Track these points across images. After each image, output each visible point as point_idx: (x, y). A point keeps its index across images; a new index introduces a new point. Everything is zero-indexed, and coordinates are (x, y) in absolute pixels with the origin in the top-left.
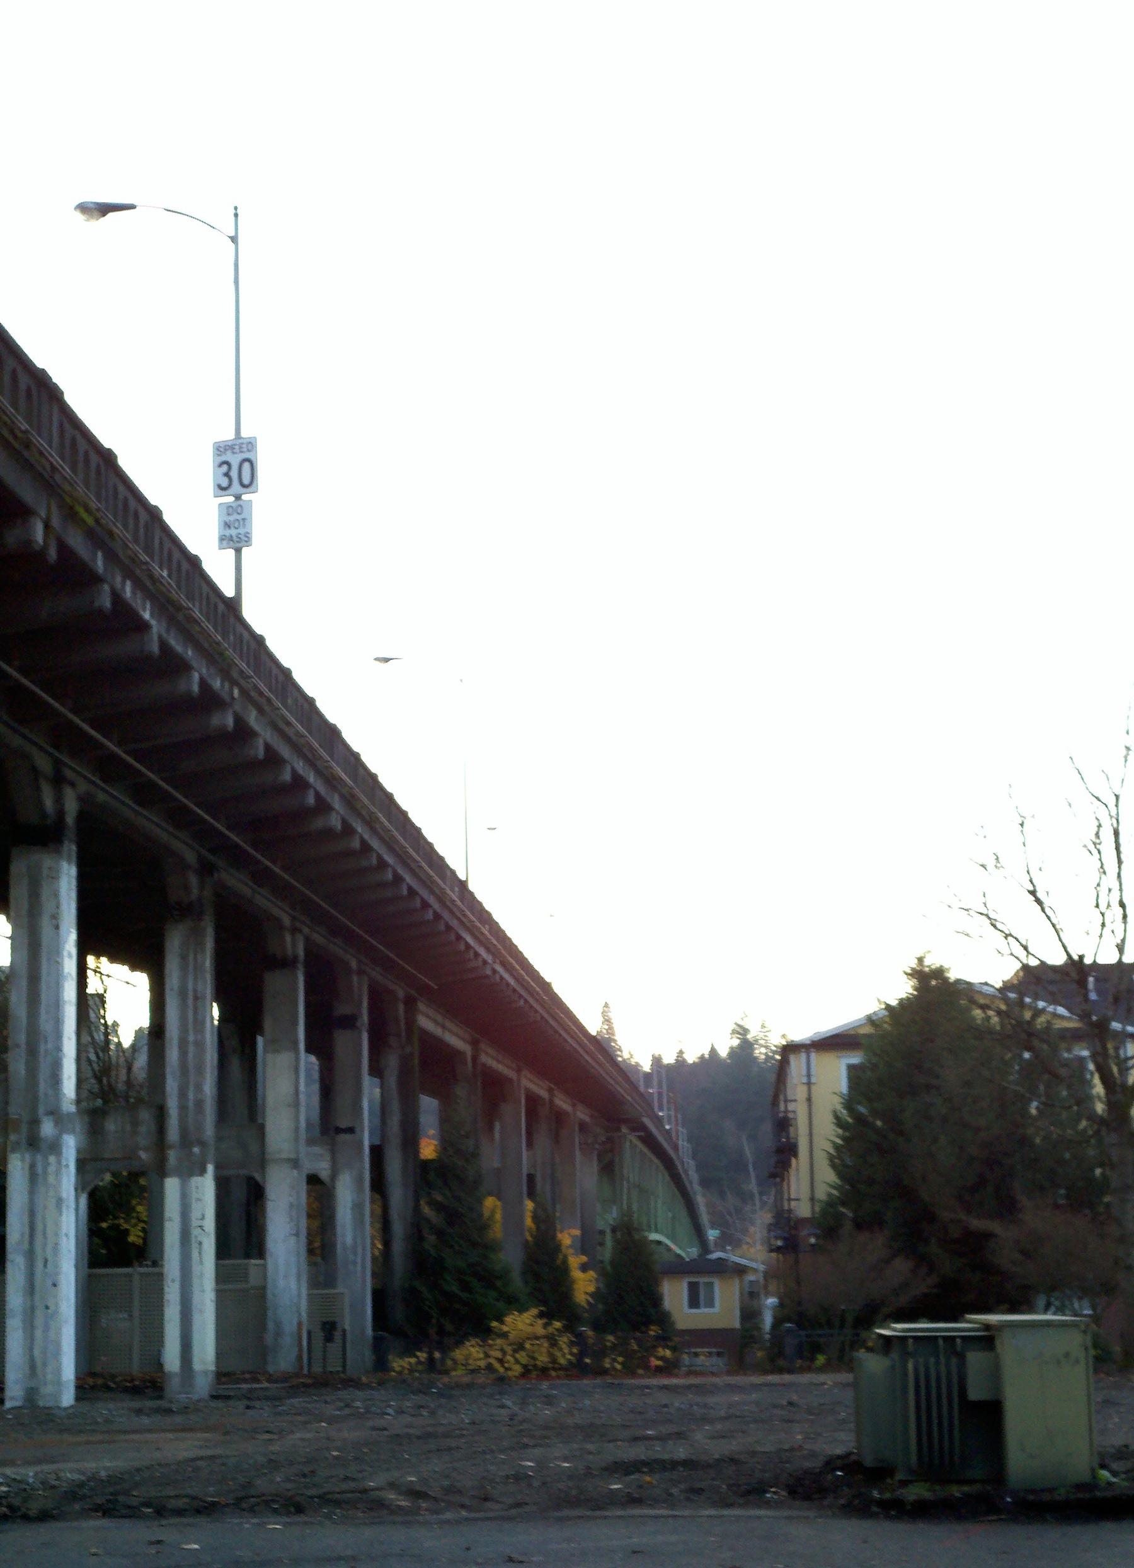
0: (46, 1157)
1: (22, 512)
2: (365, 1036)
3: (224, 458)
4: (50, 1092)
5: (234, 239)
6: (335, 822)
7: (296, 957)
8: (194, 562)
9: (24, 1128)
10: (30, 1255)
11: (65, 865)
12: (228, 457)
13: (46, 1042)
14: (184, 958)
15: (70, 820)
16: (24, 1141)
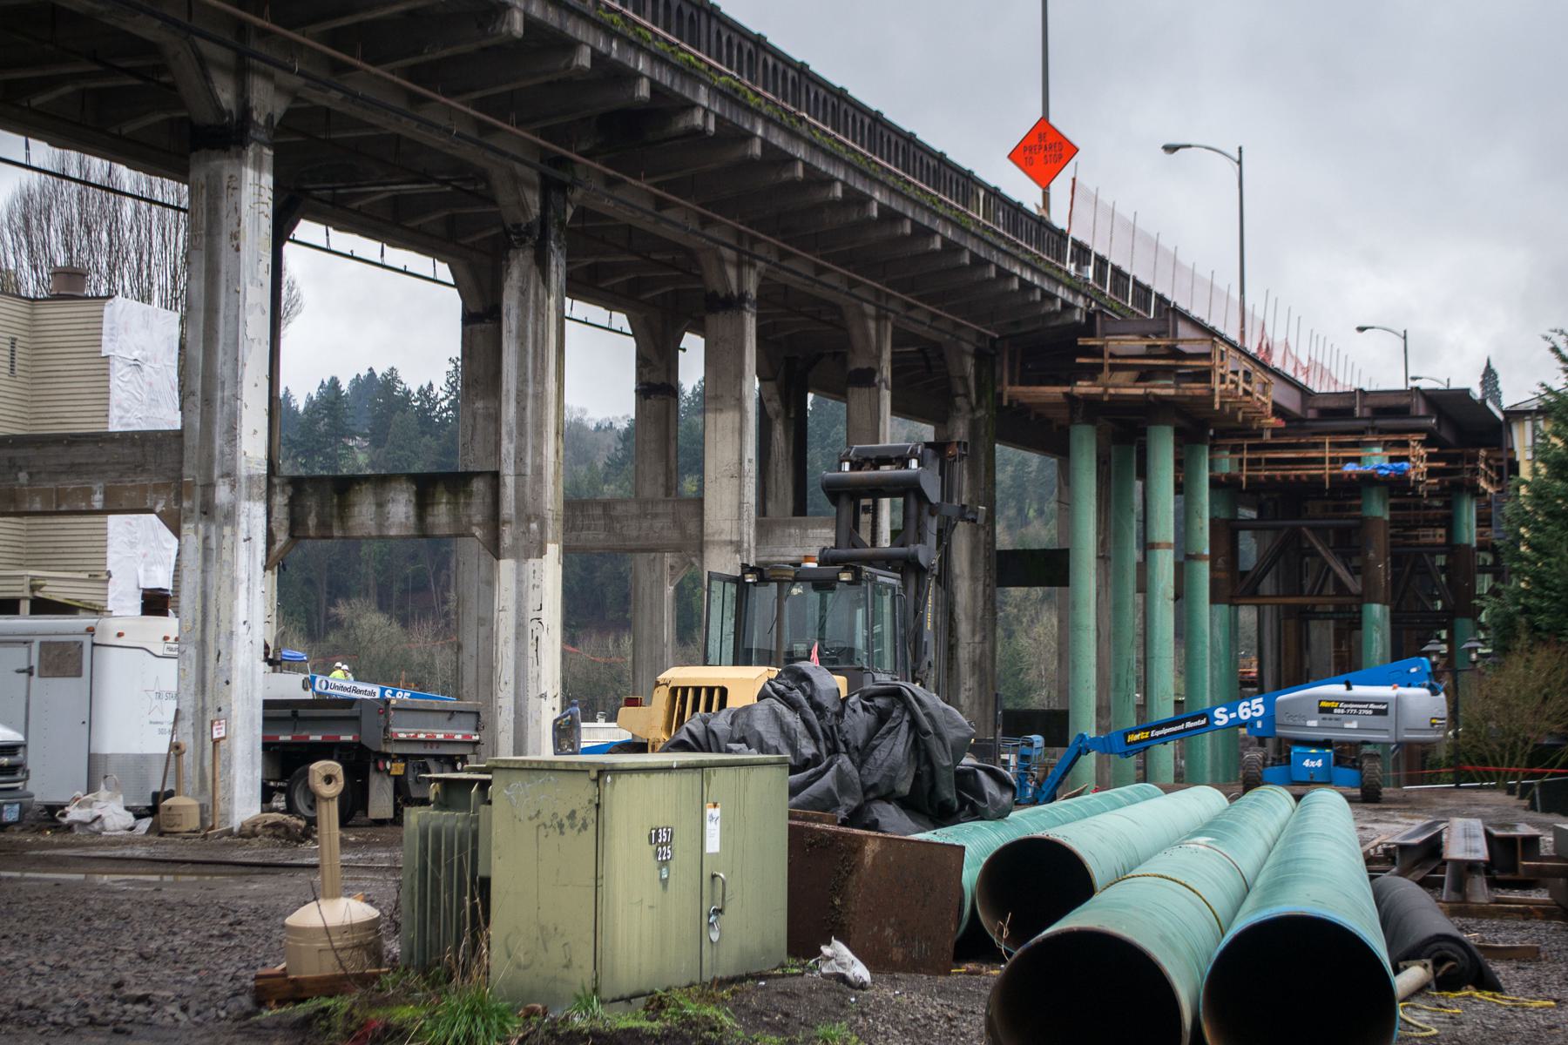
0: (220, 527)
4: (227, 450)
5: (1240, 163)
7: (742, 297)
9: (198, 491)
11: (249, 174)
13: (223, 390)
14: (523, 292)
16: (197, 510)
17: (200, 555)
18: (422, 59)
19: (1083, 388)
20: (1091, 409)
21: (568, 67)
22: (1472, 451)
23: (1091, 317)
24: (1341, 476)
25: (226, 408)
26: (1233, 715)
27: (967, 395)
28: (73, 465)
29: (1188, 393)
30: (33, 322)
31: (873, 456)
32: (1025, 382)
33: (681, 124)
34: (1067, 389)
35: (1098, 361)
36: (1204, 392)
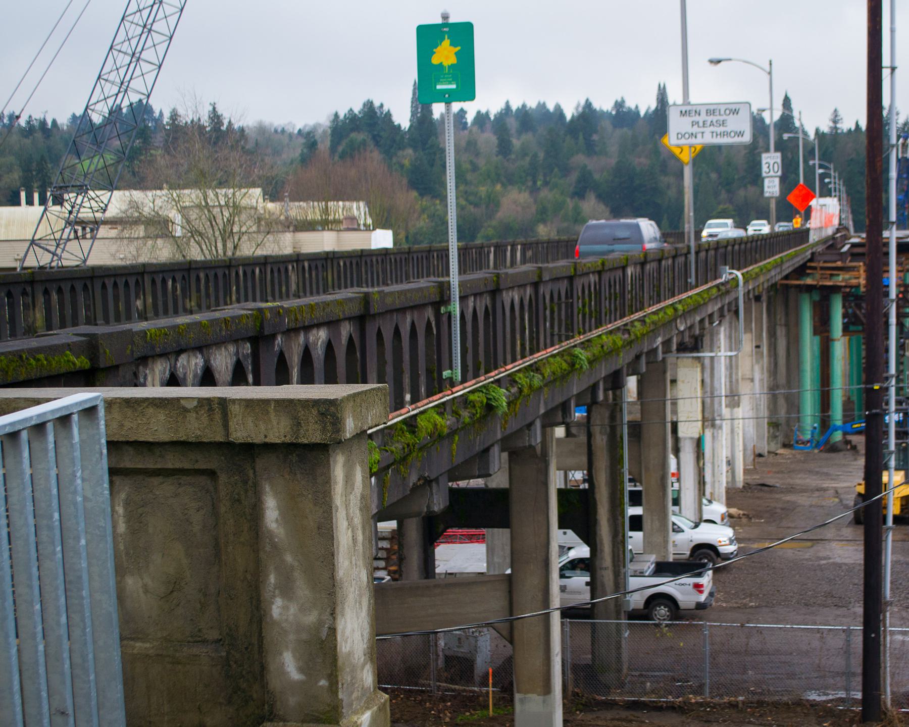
5: (770, 73)
10: (713, 463)
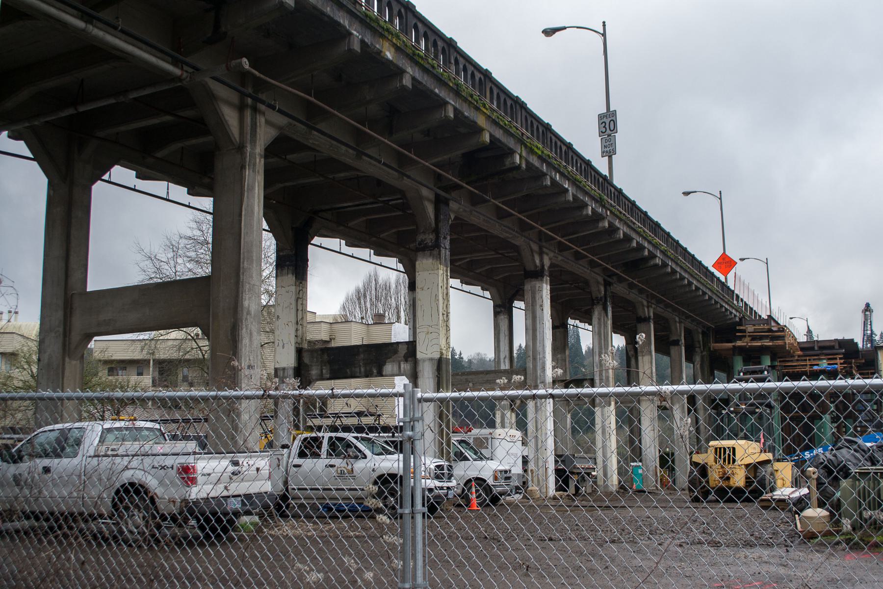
1: (511, 152)
2: (683, 348)
3: (603, 121)
4: (542, 374)
6: (658, 261)
7: (649, 317)
8: (588, 163)
11: (545, 285)
12: (605, 120)
14: (599, 319)
15: (546, 268)
17: (534, 409)
18: (589, 246)
19: (739, 343)
20: (741, 350)
21: (629, 247)
22: (850, 360)
23: (741, 319)
24: (814, 370)
25: (541, 361)
26: (812, 454)
27: (700, 347)
28: (487, 380)
29: (777, 344)
30: (368, 331)
31: (750, 370)
32: (716, 342)
33: (652, 263)
34: (734, 344)
35: (744, 334)
36: (782, 344)
